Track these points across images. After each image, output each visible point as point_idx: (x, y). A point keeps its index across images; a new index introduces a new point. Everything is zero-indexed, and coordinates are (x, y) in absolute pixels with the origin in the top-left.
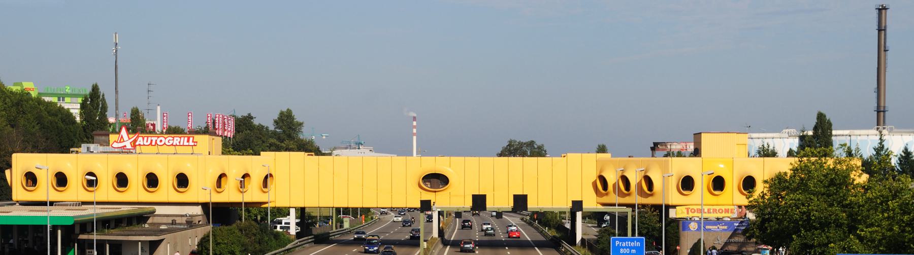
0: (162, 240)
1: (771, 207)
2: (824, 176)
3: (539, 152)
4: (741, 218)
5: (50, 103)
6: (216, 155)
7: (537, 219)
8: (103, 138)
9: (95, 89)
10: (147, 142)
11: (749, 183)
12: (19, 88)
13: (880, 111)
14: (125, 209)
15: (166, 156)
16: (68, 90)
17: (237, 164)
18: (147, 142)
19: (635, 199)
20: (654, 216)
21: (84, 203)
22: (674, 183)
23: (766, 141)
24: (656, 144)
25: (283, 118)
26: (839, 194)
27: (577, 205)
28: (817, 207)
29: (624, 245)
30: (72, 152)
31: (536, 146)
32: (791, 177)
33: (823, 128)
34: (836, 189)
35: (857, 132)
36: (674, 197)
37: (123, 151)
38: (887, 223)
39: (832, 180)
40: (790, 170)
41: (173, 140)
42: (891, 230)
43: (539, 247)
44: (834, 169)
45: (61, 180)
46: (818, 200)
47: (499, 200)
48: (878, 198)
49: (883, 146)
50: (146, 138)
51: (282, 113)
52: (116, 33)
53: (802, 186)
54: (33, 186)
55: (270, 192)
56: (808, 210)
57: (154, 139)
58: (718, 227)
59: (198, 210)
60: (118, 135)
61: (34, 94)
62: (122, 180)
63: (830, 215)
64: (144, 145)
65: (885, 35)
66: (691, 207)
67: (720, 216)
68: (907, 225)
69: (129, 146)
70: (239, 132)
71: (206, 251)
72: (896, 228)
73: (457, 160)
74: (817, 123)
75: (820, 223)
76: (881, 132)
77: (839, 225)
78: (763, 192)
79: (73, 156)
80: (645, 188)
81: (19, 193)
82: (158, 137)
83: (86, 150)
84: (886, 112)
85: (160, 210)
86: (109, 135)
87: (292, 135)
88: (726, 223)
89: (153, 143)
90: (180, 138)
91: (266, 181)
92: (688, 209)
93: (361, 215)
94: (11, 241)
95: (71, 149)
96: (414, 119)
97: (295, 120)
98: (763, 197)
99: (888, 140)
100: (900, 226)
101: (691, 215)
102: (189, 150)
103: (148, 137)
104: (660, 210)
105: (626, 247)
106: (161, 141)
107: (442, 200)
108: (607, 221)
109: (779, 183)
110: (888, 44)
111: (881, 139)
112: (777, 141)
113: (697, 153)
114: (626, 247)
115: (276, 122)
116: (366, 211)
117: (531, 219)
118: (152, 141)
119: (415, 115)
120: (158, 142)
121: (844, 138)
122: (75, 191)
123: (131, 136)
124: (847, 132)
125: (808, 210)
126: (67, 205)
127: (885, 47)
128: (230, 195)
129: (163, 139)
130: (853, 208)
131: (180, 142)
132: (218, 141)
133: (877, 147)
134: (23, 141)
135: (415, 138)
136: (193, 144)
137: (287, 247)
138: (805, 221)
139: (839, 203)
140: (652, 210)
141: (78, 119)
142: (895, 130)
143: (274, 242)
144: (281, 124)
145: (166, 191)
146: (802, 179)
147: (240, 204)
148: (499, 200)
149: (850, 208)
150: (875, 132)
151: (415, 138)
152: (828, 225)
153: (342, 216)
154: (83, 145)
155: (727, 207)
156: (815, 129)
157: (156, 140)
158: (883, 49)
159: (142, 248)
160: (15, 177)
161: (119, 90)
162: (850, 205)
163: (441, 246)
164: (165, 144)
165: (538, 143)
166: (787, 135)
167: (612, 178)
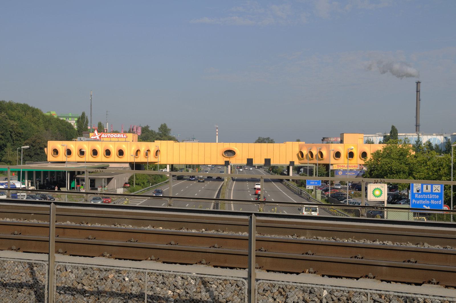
0: (112, 178)
1: (374, 165)
2: (398, 151)
3: (272, 142)
4: (361, 169)
5: (63, 120)
6: (135, 142)
7: (272, 170)
8: (87, 134)
9: (83, 114)
10: (106, 136)
11: (364, 155)
12: (49, 114)
13: (417, 126)
14: (96, 164)
15: (114, 142)
16: (70, 115)
17: (144, 146)
18: (106, 136)
19: (315, 161)
20: (324, 168)
21: (78, 162)
22: (332, 154)
23: (371, 138)
24: (324, 138)
25: (162, 127)
26: (404, 159)
27: (292, 163)
28: (395, 165)
30: (73, 140)
31: (270, 140)
32: (383, 152)
33: (394, 132)
34: (403, 157)
35: (408, 134)
36: (332, 161)
37: (95, 140)
38: (427, 171)
39: (401, 153)
40: (383, 149)
41: (117, 135)
42: (428, 174)
43: (273, 181)
44: (402, 148)
45: (69, 152)
46: (395, 162)
47: (259, 161)
48: (422, 161)
49: (419, 141)
50: (105, 135)
51: (162, 125)
52: (91, 91)
53: (388, 156)
54: (56, 155)
55: (148, 158)
56: (391, 166)
57: (109, 135)
58: (351, 174)
59: (127, 165)
60: (93, 133)
61: (55, 116)
62: (95, 152)
63: (401, 168)
64: (105, 137)
65: (419, 94)
66: (339, 165)
67: (352, 168)
68: (435, 172)
69: (98, 138)
70: (143, 133)
71: (132, 182)
72: (430, 173)
74: (392, 130)
75: (396, 172)
76: (418, 134)
77: (404, 173)
78: (371, 158)
79: (74, 142)
80: (320, 157)
81: (50, 158)
82: (111, 134)
83: (80, 140)
84: (420, 126)
85: (111, 165)
86: (89, 133)
87: (166, 134)
88: (355, 172)
89: (109, 137)
90: (120, 134)
91: (157, 152)
92: (338, 166)
93: (196, 168)
94: (47, 178)
95: (73, 139)
96: (217, 128)
97: (167, 128)
98: (371, 160)
99: (421, 138)
100: (432, 172)
101: (339, 168)
102: (124, 140)
103: (106, 134)
104: (327, 166)
106: (112, 136)
107: (234, 161)
108: (301, 171)
109: (377, 155)
110: (420, 98)
111: (418, 137)
112: (374, 138)
113: (342, 142)
115: (159, 129)
116: (198, 166)
117: (269, 170)
119: (218, 127)
121: (402, 137)
122: (75, 157)
123: (99, 134)
124: (404, 134)
125: (391, 166)
126: (71, 163)
127: (419, 99)
128: (141, 159)
129: (113, 135)
130: (411, 165)
131: (120, 136)
132: (136, 136)
133: (417, 140)
134: (51, 136)
135: (217, 136)
137: (166, 181)
138: (390, 170)
139: (404, 163)
140: (323, 166)
141: (76, 127)
142: (424, 134)
143: (160, 179)
144: (161, 130)
145: (114, 157)
146: (388, 153)
147: (147, 163)
148: (259, 161)
149: (409, 165)
150: (416, 134)
151: (217, 136)
152: (400, 172)
153: (188, 168)
154: (78, 137)
155: (355, 165)
156: (391, 132)
157: (110, 135)
158: (418, 99)
159: (104, 181)
160: (49, 151)
161: (92, 114)
162: (409, 164)
163: (232, 181)
164: (114, 137)
165: (271, 138)
166: (378, 135)
167: (305, 152)
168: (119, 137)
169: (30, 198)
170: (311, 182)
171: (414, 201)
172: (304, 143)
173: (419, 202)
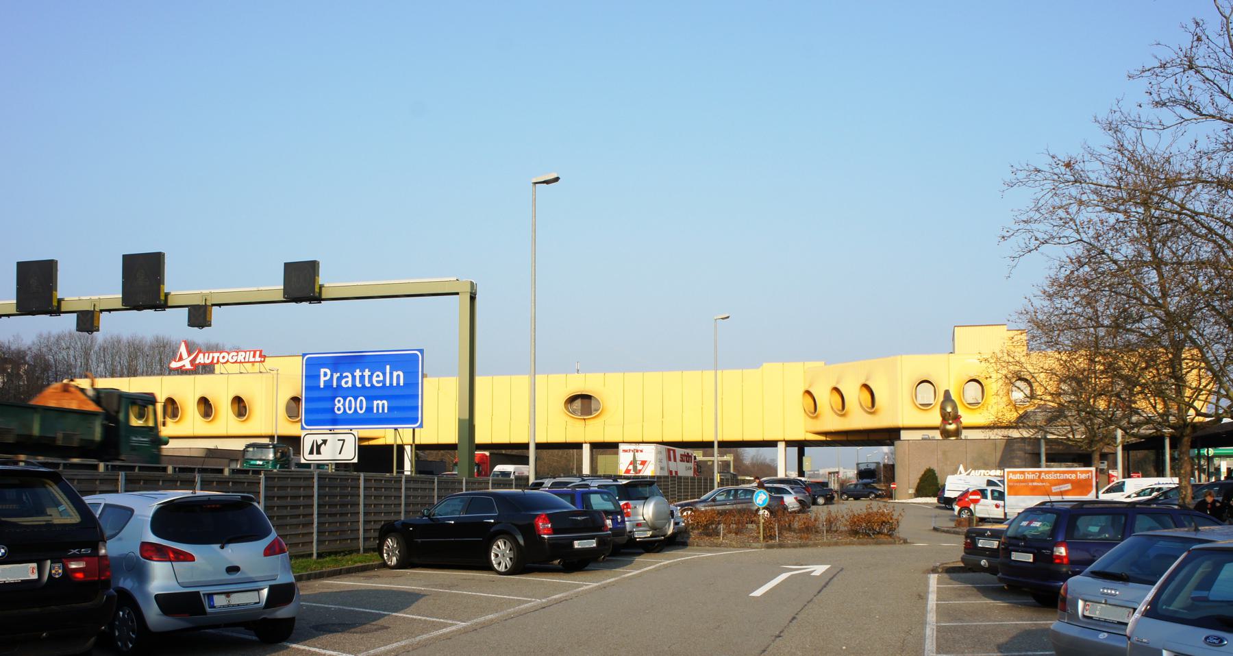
29: (347, 382)
69: (188, 366)
73: (614, 378)
82: (221, 353)
105: (354, 391)
106: (223, 357)
114: (354, 391)
118: (213, 358)
120: (221, 360)
136: (259, 359)
145: (226, 421)
157: (218, 357)
168: (241, 362)
169: (1157, 529)
170: (339, 404)
171: (325, 375)
172: (821, 364)
173: (354, 377)
